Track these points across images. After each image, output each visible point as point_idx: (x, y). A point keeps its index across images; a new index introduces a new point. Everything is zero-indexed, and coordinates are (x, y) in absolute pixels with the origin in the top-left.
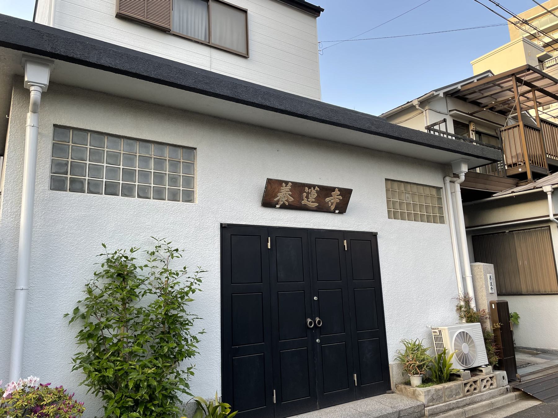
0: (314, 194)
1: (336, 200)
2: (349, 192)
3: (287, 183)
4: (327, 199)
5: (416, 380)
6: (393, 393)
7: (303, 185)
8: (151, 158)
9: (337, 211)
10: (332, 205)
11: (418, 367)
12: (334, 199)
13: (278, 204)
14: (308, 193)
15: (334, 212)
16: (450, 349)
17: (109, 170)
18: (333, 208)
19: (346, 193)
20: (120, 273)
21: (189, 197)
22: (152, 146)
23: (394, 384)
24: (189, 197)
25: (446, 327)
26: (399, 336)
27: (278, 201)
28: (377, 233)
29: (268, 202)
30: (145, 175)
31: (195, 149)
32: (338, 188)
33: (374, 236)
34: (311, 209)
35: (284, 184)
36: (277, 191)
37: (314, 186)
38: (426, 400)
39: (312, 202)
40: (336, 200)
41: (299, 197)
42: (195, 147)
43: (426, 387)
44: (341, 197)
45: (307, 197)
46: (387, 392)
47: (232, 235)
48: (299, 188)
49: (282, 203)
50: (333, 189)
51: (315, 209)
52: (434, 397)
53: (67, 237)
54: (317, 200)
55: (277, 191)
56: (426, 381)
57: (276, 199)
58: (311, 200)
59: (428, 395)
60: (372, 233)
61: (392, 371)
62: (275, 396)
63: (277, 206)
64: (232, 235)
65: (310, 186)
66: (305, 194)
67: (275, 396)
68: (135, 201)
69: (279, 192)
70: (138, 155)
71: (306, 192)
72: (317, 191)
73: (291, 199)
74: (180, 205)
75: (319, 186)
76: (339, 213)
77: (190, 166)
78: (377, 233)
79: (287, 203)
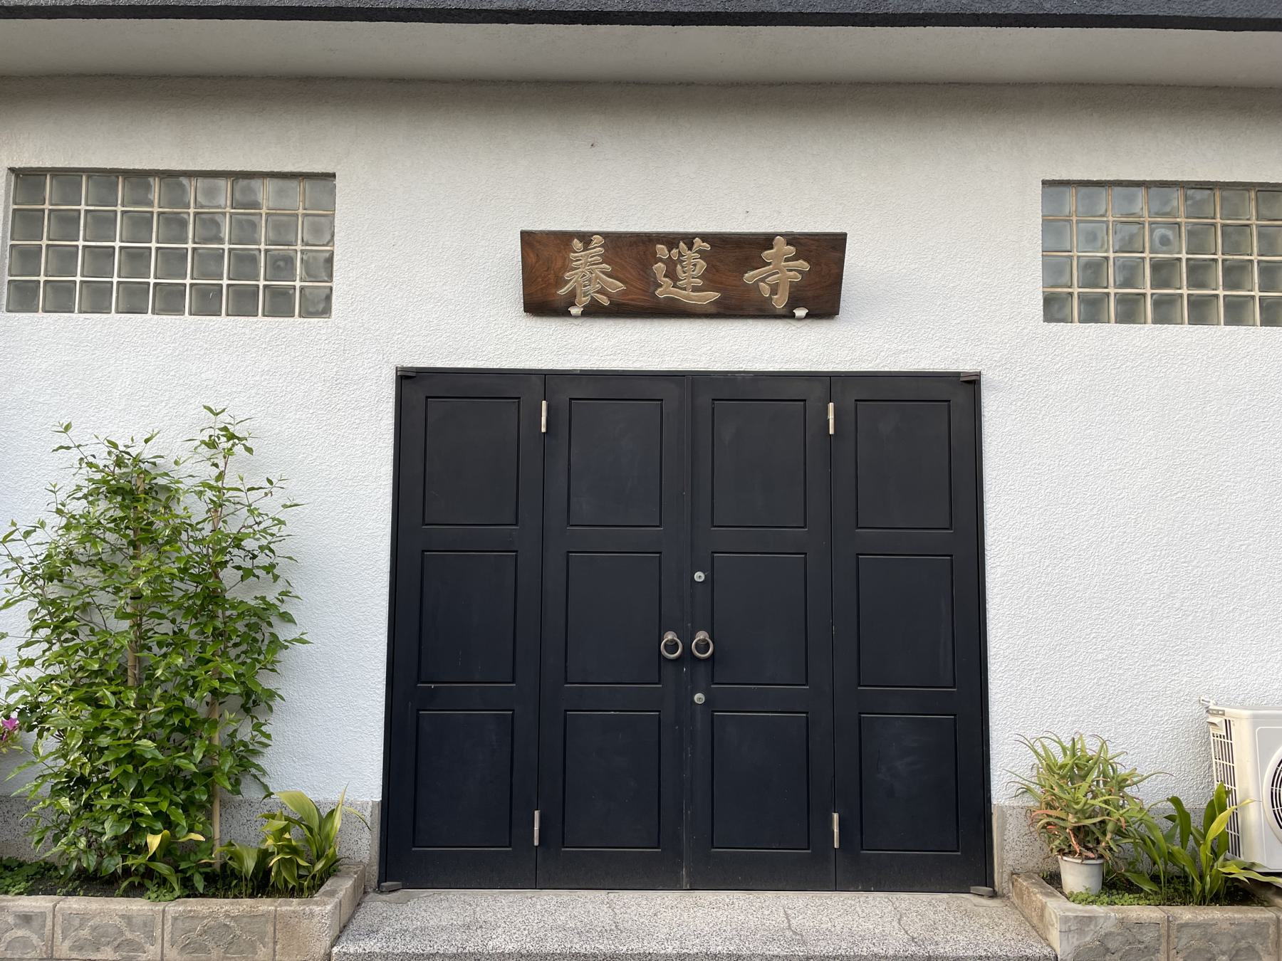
0: (693, 265)
1: (819, 274)
2: (837, 243)
3: (586, 238)
4: (750, 277)
5: (1076, 875)
6: (994, 895)
7: (648, 240)
8: (224, 214)
9: (800, 312)
10: (774, 290)
11: (1077, 830)
12: (780, 273)
13: (573, 304)
14: (671, 266)
15: (789, 315)
16: (1253, 794)
17: (1157, 267)
18: (780, 302)
19: (824, 253)
20: (133, 493)
21: (319, 306)
22: (1141, 192)
23: (1008, 870)
24: (319, 306)
25: (1248, 713)
26: (1029, 720)
27: (573, 294)
28: (979, 375)
29: (542, 301)
30: (136, 259)
31: (334, 175)
32: (781, 235)
33: (968, 387)
34: (698, 311)
35: (577, 244)
36: (559, 264)
37: (689, 239)
38: (1069, 949)
39: (695, 289)
40: (819, 274)
41: (639, 276)
42: (331, 171)
43: (1112, 903)
44: (804, 265)
45: (671, 275)
46: (973, 889)
47: (428, 401)
48: (632, 251)
49: (586, 300)
50: (766, 241)
51: (713, 310)
52: (1112, 945)
53: (33, 411)
54: (710, 280)
55: (559, 264)
56: (1114, 884)
57: (563, 291)
58: (689, 281)
59: (1081, 932)
60: (957, 375)
61: (1003, 829)
62: (536, 828)
63: (574, 311)
64: (428, 401)
65: (671, 240)
66: (659, 268)
67: (536, 828)
68: (186, 322)
69: (566, 268)
70: (1074, 219)
71: (661, 260)
72: (701, 252)
73: (616, 286)
74: (294, 325)
75: (705, 237)
76: (808, 316)
77: (324, 227)
78: (979, 375)
79: (605, 301)
